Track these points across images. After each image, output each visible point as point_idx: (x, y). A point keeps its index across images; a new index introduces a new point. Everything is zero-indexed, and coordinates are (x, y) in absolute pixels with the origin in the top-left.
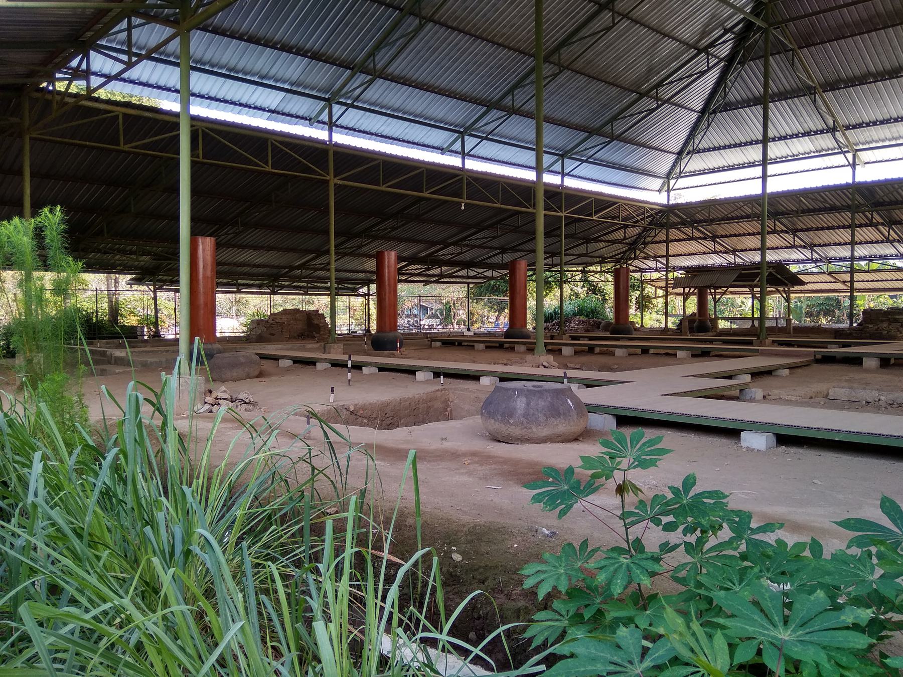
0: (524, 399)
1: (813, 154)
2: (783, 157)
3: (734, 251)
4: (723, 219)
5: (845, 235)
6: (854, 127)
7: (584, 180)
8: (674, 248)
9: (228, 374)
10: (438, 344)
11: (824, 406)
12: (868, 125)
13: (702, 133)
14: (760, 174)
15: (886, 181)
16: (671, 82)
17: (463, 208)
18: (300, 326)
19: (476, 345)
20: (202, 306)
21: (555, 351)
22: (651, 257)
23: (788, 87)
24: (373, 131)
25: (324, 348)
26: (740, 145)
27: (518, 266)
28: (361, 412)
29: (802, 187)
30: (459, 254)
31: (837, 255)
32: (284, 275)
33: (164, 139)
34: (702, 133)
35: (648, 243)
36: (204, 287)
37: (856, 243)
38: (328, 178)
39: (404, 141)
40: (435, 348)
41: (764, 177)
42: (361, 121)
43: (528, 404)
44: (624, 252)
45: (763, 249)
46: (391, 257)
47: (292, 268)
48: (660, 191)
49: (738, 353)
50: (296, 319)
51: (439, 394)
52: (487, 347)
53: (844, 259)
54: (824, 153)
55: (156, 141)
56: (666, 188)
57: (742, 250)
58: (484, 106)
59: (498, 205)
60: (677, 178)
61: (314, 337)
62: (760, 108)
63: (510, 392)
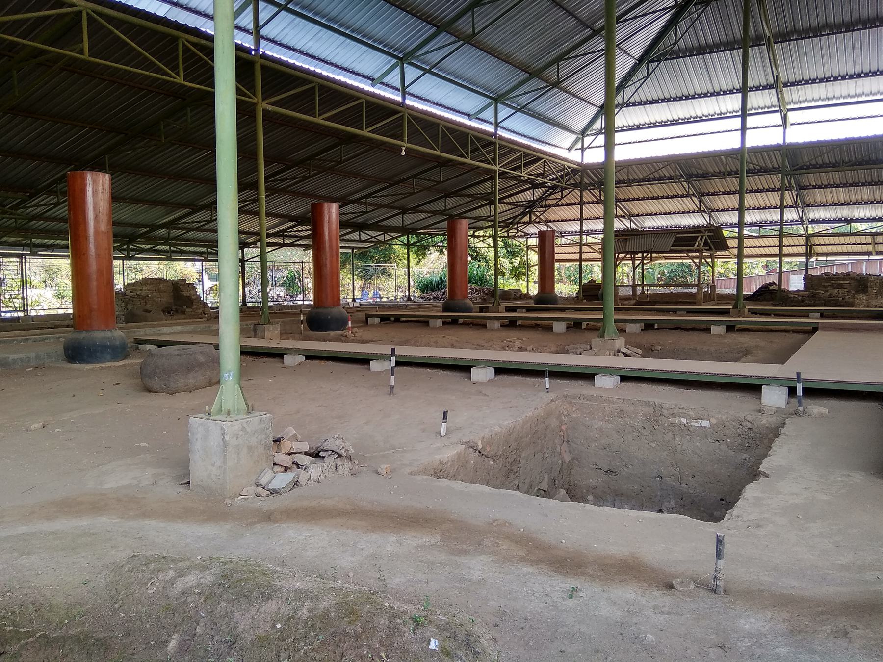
1: (716, 116)
2: (697, 117)
3: (630, 216)
4: (643, 180)
5: (575, 211)
6: (793, 84)
7: (518, 129)
8: (750, 200)
9: (181, 382)
10: (377, 320)
12: (807, 83)
13: (638, 84)
14: (739, 126)
15: (819, 142)
16: (626, 21)
17: (403, 153)
18: (165, 299)
20: (94, 276)
23: (725, 39)
24: (298, 47)
25: (255, 330)
27: (459, 226)
31: (770, 219)
32: (142, 236)
33: (28, 19)
34: (638, 84)
35: (550, 206)
36: (97, 248)
37: (786, 207)
38: (255, 100)
39: (331, 64)
40: (373, 325)
41: (743, 129)
42: (286, 31)
45: (741, 209)
46: (332, 212)
47: (155, 227)
50: (160, 291)
52: (444, 323)
53: (572, 234)
55: (15, 21)
56: (579, 145)
57: (554, 221)
58: (434, 25)
59: (438, 153)
61: (183, 313)
62: (738, 54)
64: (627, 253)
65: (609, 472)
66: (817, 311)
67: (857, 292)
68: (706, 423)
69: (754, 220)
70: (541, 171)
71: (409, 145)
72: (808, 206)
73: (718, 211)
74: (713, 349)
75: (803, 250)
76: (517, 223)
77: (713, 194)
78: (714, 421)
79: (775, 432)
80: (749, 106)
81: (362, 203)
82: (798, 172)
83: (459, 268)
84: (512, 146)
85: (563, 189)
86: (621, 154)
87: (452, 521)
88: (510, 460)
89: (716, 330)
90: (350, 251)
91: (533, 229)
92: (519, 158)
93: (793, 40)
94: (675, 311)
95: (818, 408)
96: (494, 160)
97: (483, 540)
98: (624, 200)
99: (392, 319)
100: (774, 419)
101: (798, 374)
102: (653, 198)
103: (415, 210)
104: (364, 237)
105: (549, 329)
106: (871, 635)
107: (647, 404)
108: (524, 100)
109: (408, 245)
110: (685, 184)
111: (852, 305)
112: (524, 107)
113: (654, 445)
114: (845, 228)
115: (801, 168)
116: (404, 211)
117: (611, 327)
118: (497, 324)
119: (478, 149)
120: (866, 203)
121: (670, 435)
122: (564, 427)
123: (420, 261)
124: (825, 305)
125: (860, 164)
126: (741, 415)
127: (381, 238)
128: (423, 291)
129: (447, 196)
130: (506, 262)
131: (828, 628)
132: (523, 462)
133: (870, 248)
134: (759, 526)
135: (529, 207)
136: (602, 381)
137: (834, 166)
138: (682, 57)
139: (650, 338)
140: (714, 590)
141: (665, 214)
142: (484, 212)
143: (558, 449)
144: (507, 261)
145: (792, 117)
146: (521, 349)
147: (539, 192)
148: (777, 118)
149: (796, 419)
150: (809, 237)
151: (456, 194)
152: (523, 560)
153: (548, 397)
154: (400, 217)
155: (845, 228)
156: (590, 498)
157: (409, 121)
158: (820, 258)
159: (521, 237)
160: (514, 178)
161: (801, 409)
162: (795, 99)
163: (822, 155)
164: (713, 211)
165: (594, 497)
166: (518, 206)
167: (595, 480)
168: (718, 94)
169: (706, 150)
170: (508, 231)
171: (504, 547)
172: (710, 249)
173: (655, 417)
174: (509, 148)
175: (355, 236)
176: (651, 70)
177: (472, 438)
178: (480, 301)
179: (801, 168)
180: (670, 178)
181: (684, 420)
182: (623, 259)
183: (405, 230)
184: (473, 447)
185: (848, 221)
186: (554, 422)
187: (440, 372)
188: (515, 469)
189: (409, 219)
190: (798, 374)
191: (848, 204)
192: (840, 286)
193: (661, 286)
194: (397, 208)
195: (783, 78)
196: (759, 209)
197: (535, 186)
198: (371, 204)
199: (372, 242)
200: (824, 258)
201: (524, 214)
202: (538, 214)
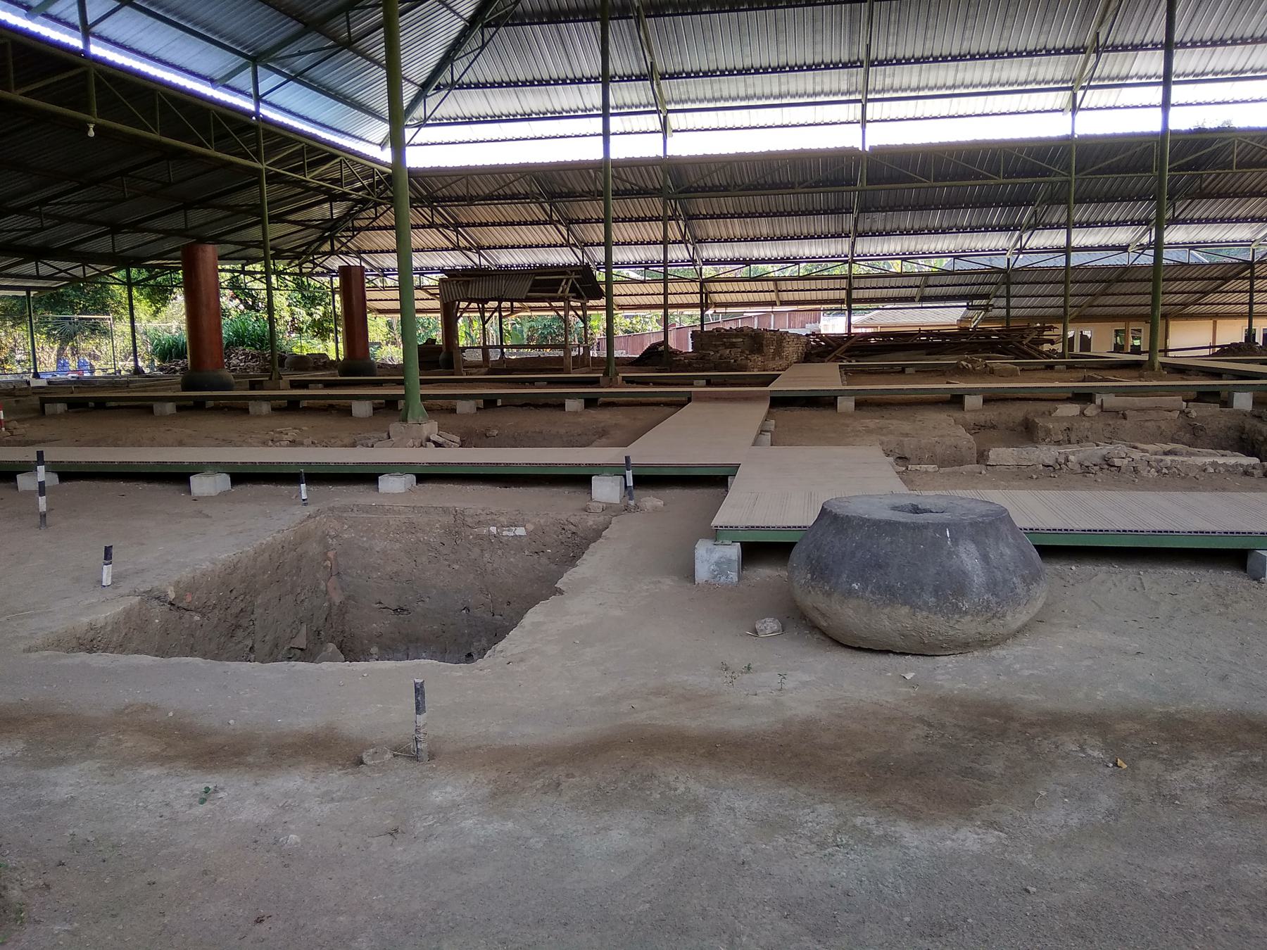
0: (972, 547)
1: (580, 113)
2: (554, 112)
3: (479, 248)
6: (672, 77)
7: (291, 107)
8: (621, 231)
11: (1155, 486)
13: (472, 56)
15: (738, 155)
17: (92, 133)
19: (157, 407)
21: (439, 409)
22: (354, 252)
26: (541, 83)
28: (189, 599)
29: (464, 164)
30: (36, 230)
34: (472, 56)
35: (360, 229)
40: (54, 416)
41: (1166, 105)
43: (985, 558)
44: (310, 244)
48: (382, 145)
49: (652, 399)
51: (311, 524)
52: (179, 408)
54: (626, 110)
57: (370, 252)
59: (155, 136)
60: (419, 126)
63: (930, 533)
64: (470, 301)
65: (399, 610)
66: (702, 377)
67: (752, 352)
68: (521, 531)
69: (638, 259)
70: (337, 175)
71: (101, 121)
72: (700, 242)
73: (592, 245)
74: (562, 431)
75: (696, 299)
76: (313, 253)
77: (584, 222)
78: (530, 527)
79: (597, 534)
80: (612, 102)
81: (35, 214)
82: (683, 195)
83: (205, 322)
84: (286, 133)
85: (376, 205)
86: (416, 159)
87: (53, 717)
88: (234, 610)
89: (571, 405)
90: (24, 293)
91: (336, 263)
92: (300, 154)
93: (669, 15)
94: (532, 382)
95: (651, 500)
96: (257, 153)
97: (98, 738)
98: (468, 225)
99: (92, 404)
100: (602, 518)
101: (627, 459)
102: (506, 224)
103: (135, 227)
104: (45, 270)
105: (347, 411)
106: (587, 781)
107: (445, 511)
108: (301, 63)
109: (129, 284)
110: (547, 206)
111: (744, 368)
112: (301, 74)
113: (456, 567)
114: (743, 272)
115: (687, 191)
116: (115, 229)
117: (417, 406)
118: (265, 408)
119: (227, 135)
120: (766, 239)
121: (477, 550)
122: (331, 554)
123: (157, 311)
124: (716, 370)
125: (756, 188)
126: (563, 516)
127: (78, 272)
128: (163, 359)
129: (188, 206)
130: (286, 309)
131: (539, 783)
132: (258, 611)
133: (773, 296)
134: (522, 660)
135: (328, 230)
136: (391, 485)
137: (726, 189)
138: (529, 24)
139: (489, 420)
140: (415, 757)
141: (525, 247)
142: (255, 233)
143: (323, 587)
144: (303, 312)
145: (675, 120)
146: (293, 443)
147: (338, 210)
148: (653, 122)
149: (626, 517)
150: (703, 282)
151: (203, 203)
152: (155, 759)
153: (300, 512)
154: (108, 238)
155: (743, 272)
156: (374, 650)
157: (98, 83)
158: (718, 310)
159: (322, 274)
160: (298, 183)
161: (632, 503)
162: (676, 96)
163: (710, 174)
164: (586, 245)
165: (380, 648)
166: (308, 227)
167: (381, 624)
168: (580, 82)
169: (487, 163)
170: (300, 265)
171: (129, 744)
172: (579, 297)
173: (457, 528)
174: (280, 137)
175: (29, 268)
176: (487, 37)
177: (156, 584)
178: (258, 373)
179: (687, 191)
180: (526, 196)
181: (493, 529)
182: (465, 310)
183: (123, 261)
184: (158, 598)
185: (747, 262)
186: (314, 548)
187: (142, 487)
188: (244, 622)
189: (126, 242)
190: (627, 459)
191: (746, 240)
192: (733, 345)
193: (533, 347)
194: (100, 223)
195: (660, 67)
196: (642, 243)
197: (332, 198)
198: (48, 216)
199: (62, 279)
200: (723, 310)
201: (322, 240)
202: (344, 240)
